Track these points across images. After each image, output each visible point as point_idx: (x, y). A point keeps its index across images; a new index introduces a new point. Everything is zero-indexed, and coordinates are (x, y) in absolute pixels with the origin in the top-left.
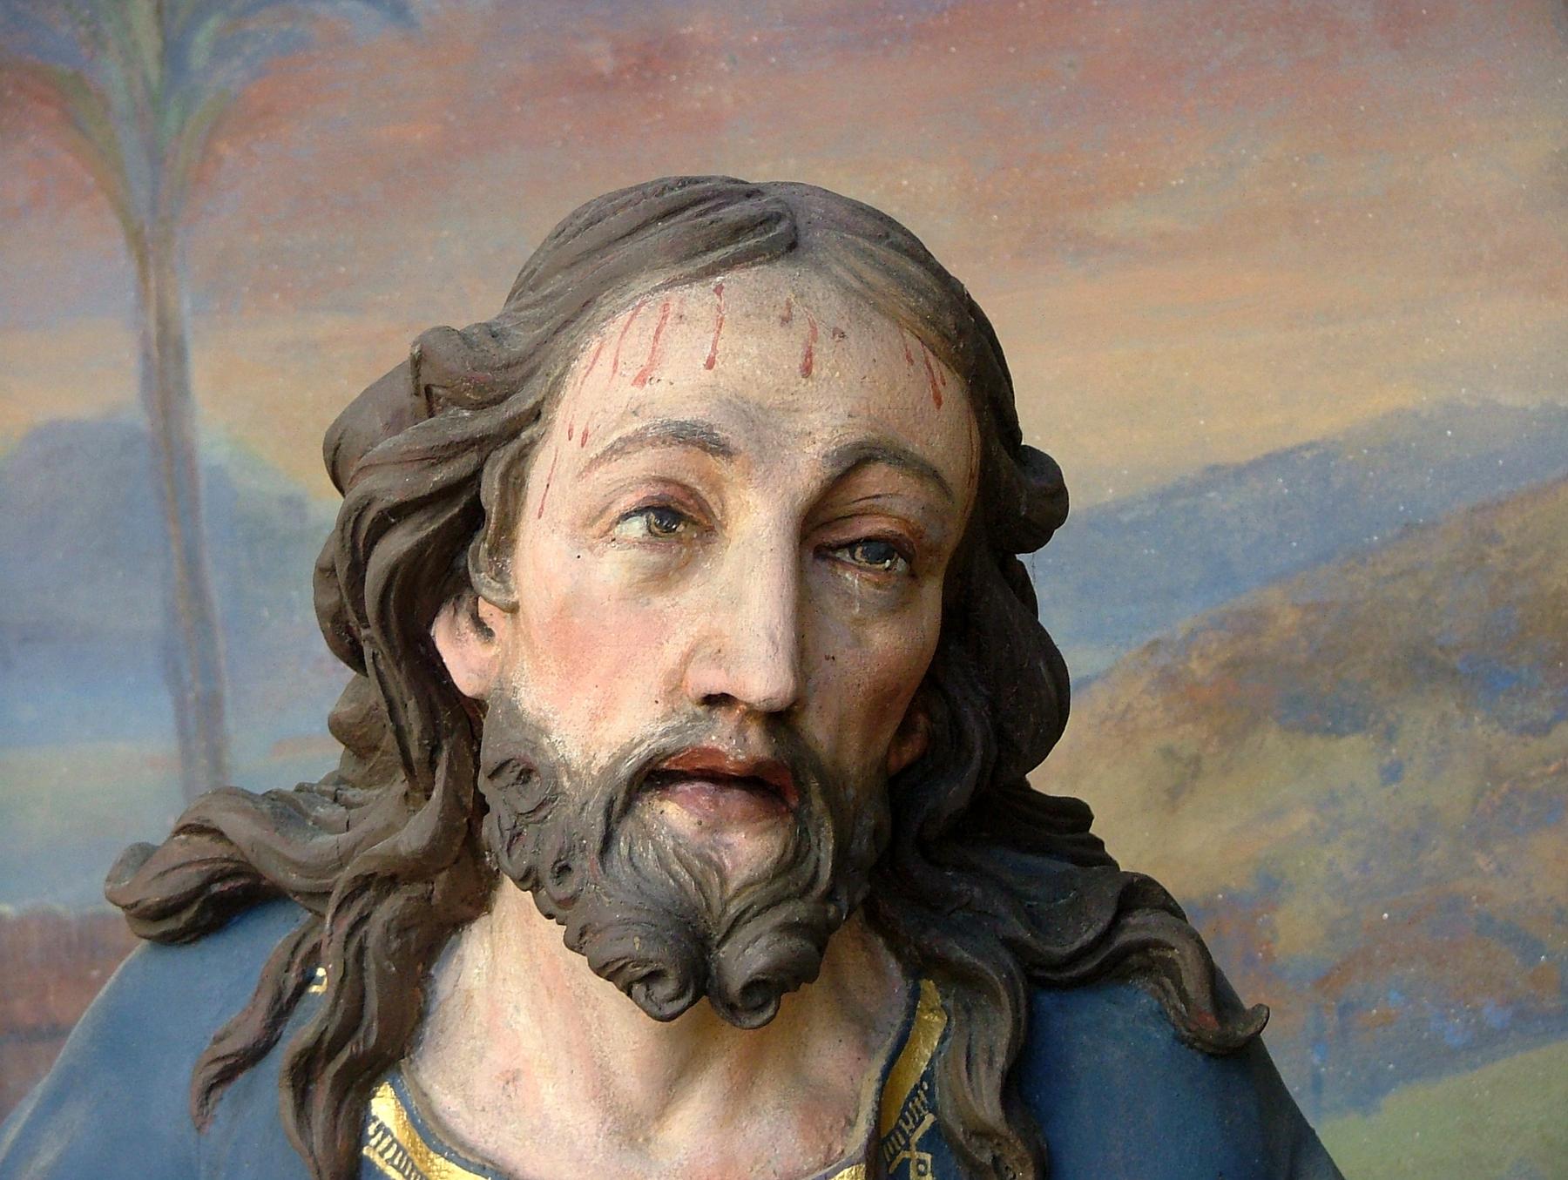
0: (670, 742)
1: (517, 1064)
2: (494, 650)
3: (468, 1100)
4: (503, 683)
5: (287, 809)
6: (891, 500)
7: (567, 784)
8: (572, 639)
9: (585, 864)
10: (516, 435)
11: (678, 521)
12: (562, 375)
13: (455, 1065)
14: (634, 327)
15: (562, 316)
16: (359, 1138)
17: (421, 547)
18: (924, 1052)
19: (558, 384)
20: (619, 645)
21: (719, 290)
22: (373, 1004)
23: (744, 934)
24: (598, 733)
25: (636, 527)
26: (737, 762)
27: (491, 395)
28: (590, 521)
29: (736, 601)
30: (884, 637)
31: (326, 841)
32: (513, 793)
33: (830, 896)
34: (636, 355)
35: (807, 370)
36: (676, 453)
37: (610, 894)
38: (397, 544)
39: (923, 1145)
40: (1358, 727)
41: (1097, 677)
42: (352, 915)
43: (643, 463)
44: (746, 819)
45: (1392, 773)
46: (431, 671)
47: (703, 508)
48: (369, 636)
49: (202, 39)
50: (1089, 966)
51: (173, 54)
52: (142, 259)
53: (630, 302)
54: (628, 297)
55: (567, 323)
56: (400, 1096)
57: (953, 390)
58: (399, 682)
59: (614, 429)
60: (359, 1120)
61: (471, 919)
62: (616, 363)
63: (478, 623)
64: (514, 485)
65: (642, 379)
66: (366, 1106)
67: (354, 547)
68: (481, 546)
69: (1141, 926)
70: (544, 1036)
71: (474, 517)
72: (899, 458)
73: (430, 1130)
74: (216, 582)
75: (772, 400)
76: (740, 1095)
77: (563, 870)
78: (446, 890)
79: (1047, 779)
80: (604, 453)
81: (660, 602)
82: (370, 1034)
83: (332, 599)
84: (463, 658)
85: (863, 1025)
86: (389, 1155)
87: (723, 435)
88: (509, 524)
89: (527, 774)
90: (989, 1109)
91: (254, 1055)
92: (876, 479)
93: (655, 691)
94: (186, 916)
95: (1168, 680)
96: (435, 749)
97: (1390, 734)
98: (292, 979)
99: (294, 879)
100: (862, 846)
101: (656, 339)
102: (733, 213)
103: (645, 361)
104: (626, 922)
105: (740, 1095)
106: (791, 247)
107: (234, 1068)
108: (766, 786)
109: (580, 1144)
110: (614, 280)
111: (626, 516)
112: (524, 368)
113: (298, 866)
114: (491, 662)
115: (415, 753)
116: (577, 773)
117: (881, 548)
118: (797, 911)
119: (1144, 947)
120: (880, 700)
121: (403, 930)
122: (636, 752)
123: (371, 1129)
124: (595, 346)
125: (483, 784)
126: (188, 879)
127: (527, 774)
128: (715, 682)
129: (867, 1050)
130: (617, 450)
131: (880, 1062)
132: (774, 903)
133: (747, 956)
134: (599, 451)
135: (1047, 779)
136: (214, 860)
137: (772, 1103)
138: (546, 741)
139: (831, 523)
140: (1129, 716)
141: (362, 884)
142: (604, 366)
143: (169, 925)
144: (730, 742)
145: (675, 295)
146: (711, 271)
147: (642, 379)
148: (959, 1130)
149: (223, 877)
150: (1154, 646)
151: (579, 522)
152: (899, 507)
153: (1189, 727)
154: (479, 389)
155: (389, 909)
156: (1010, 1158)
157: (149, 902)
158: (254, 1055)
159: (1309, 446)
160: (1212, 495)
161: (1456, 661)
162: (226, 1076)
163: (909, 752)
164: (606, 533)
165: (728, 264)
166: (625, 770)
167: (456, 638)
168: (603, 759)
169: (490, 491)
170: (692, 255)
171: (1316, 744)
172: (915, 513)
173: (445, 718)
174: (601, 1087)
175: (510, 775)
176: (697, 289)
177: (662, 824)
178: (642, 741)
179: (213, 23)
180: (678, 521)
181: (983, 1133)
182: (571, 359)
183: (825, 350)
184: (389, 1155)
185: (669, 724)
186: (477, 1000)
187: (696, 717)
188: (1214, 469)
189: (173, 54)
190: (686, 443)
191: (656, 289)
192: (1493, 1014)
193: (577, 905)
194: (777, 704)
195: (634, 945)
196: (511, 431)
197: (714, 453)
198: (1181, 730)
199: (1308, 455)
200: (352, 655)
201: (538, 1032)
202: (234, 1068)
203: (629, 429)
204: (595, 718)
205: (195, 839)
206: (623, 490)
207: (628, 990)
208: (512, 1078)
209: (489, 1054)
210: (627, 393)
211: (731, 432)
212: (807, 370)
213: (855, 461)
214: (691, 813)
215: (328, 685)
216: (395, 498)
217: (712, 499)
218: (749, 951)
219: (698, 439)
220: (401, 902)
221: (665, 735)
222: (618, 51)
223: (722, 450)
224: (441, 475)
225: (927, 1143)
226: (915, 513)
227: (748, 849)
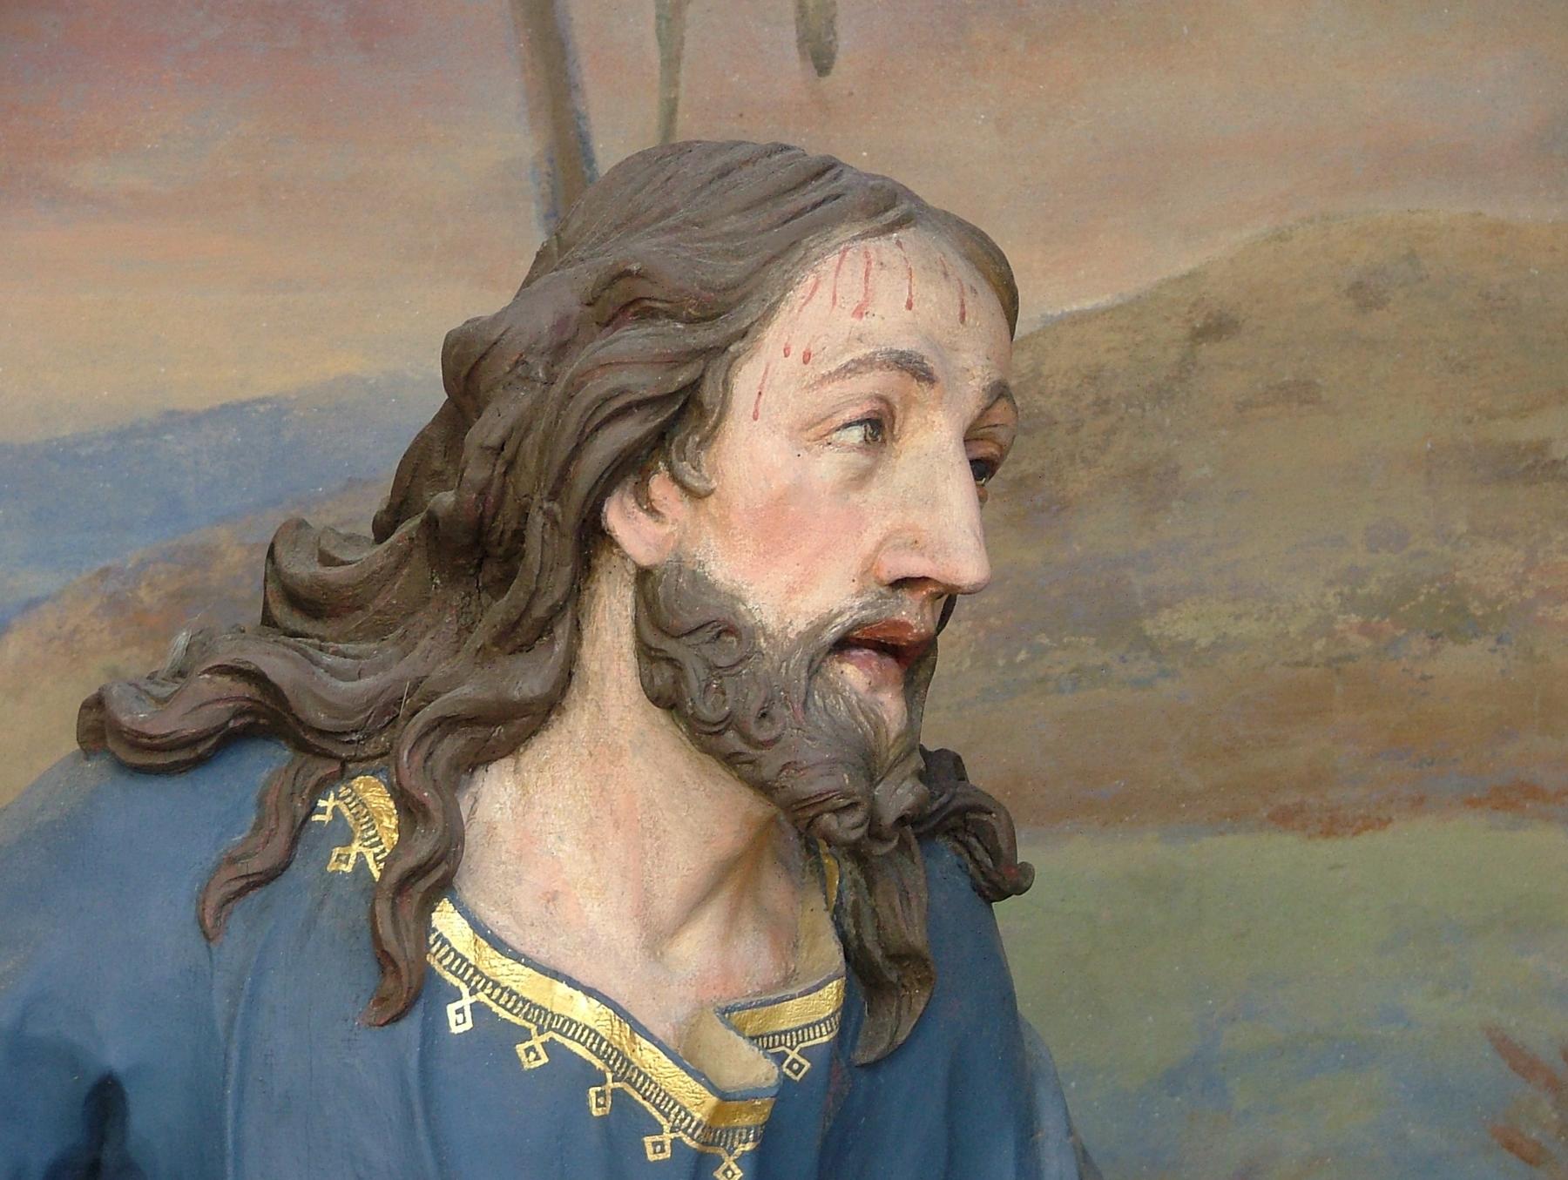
1: (557, 886)
2: (668, 529)
3: (515, 915)
7: (764, 645)
8: (779, 521)
12: (779, 301)
13: (492, 886)
14: (846, 266)
15: (768, 252)
19: (773, 308)
21: (899, 244)
24: (794, 604)
25: (856, 435)
26: (918, 635)
27: (710, 313)
28: (809, 426)
29: (931, 502)
32: (707, 650)
34: (852, 291)
36: (894, 376)
41: (47, 598)
42: (423, 751)
43: (871, 382)
53: (835, 247)
54: (834, 242)
55: (774, 258)
59: (842, 353)
62: (835, 297)
65: (860, 312)
66: (430, 921)
67: (583, 431)
70: (594, 861)
80: (838, 371)
81: (855, 498)
86: (446, 962)
87: (930, 365)
93: (854, 571)
95: (116, 605)
101: (867, 281)
103: (861, 298)
104: (834, 762)
109: (624, 954)
111: (847, 425)
113: (328, 706)
114: (666, 538)
116: (772, 636)
122: (839, 620)
123: (432, 938)
124: (811, 280)
127: (730, 630)
128: (914, 565)
134: (833, 368)
136: (237, 698)
137: (750, 926)
138: (743, 608)
140: (78, 637)
145: (872, 244)
147: (860, 312)
148: (878, 954)
150: (104, 573)
151: (798, 426)
153: (135, 650)
154: (701, 306)
157: (185, 733)
159: (263, 401)
160: (168, 437)
164: (822, 437)
167: (627, 516)
168: (801, 625)
169: (708, 393)
174: (643, 908)
177: (844, 681)
178: (840, 614)
182: (787, 289)
184: (446, 962)
185: (863, 599)
186: (501, 830)
187: (882, 596)
188: (171, 414)
190: (902, 369)
191: (855, 239)
193: (778, 745)
197: (920, 379)
198: (126, 653)
199: (261, 409)
201: (588, 858)
203: (861, 352)
204: (791, 591)
205: (218, 679)
206: (852, 403)
208: (552, 897)
209: (529, 877)
210: (847, 323)
214: (866, 675)
217: (899, 416)
218: (899, 791)
220: (461, 742)
221: (863, 608)
224: (683, 377)
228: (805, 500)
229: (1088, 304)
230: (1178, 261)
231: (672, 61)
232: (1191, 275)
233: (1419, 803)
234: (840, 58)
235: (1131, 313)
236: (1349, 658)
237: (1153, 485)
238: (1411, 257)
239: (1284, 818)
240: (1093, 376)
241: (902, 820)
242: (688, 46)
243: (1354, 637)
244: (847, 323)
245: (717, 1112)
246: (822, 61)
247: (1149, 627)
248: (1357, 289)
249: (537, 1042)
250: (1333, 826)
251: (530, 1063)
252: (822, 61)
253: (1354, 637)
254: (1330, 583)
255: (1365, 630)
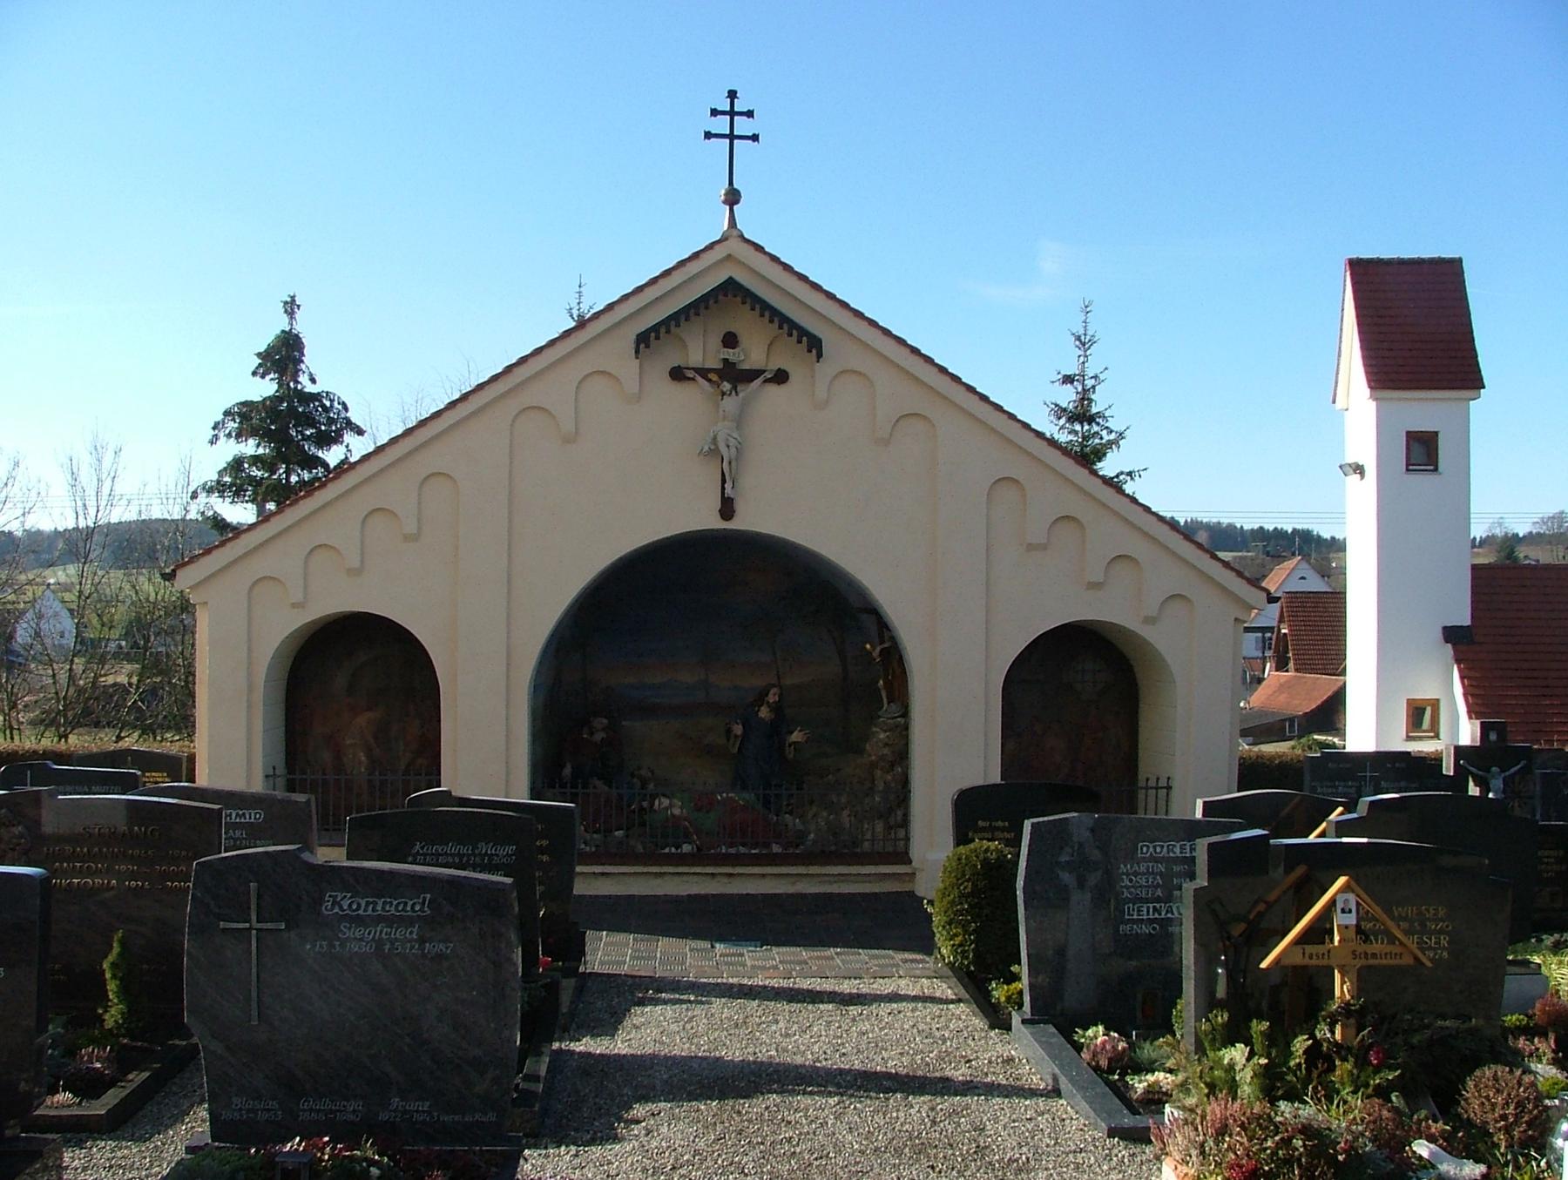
228: (772, 697)
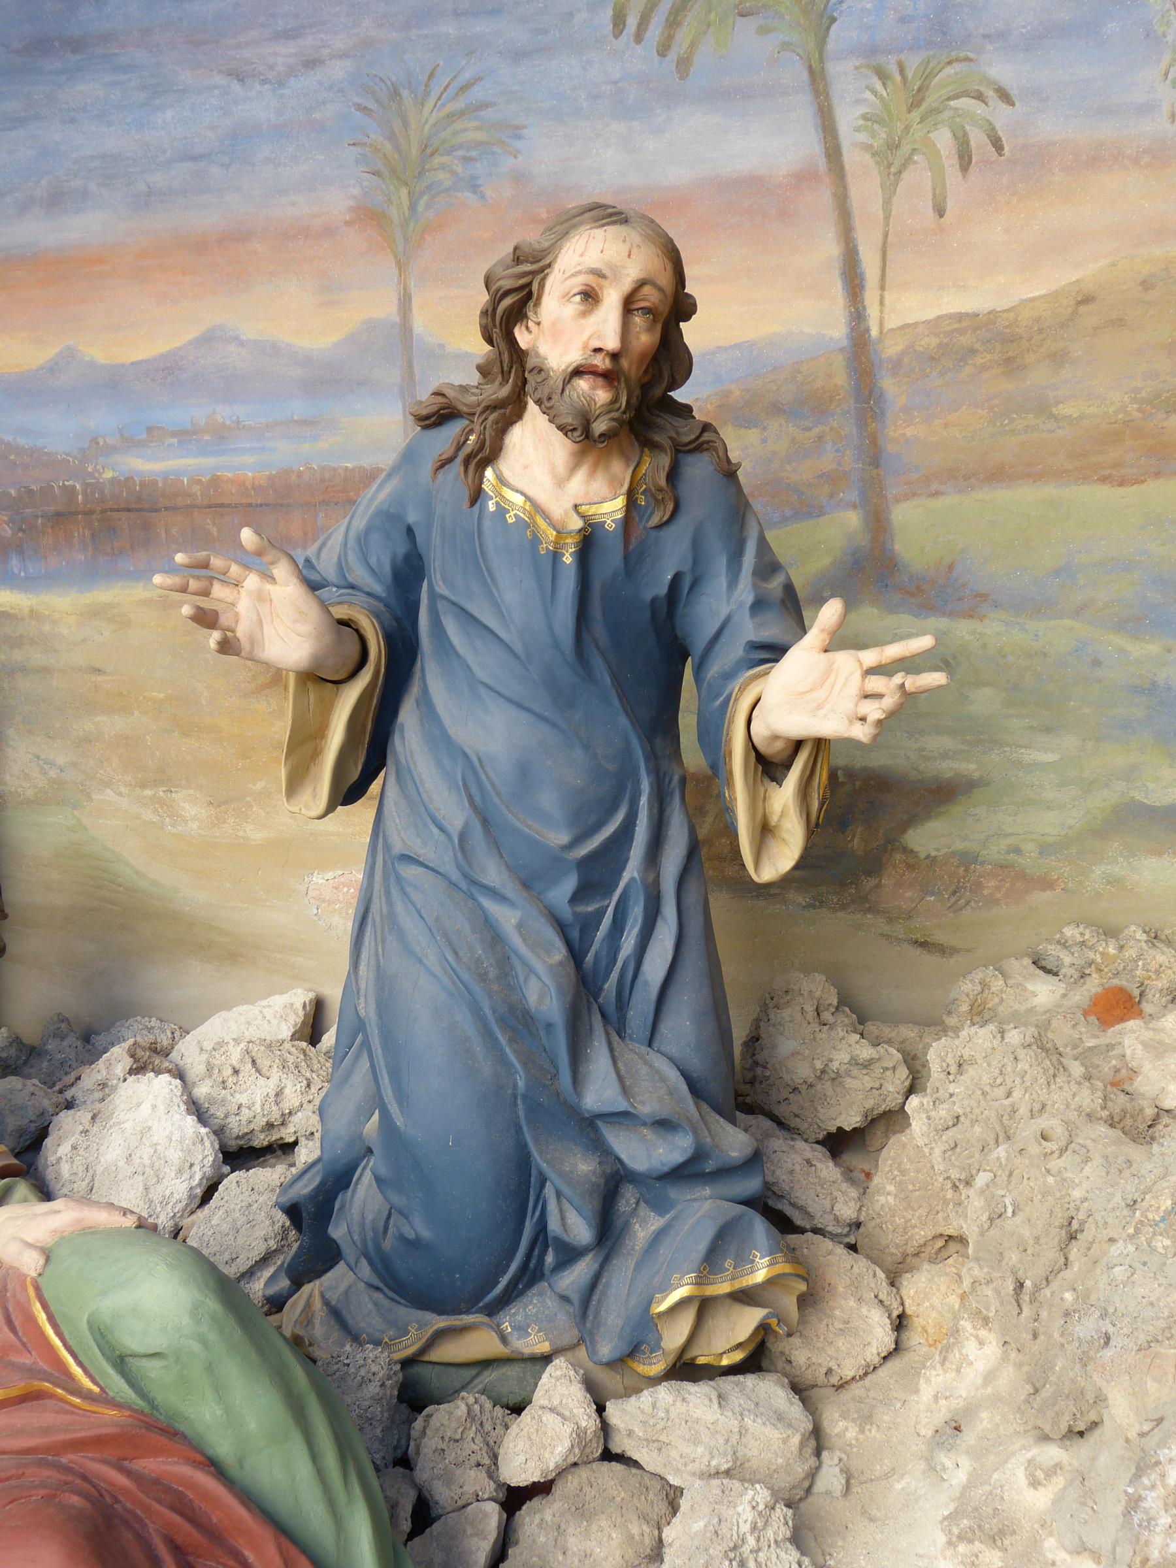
0: (584, 362)
4: (534, 346)
5: (464, 389)
6: (650, 296)
8: (556, 332)
9: (555, 397)
10: (544, 271)
11: (590, 297)
16: (481, 482)
17: (514, 303)
18: (643, 469)
19: (556, 257)
20: (568, 334)
22: (488, 443)
23: (601, 419)
28: (564, 296)
29: (605, 321)
30: (645, 339)
31: (474, 398)
33: (624, 412)
35: (629, 256)
37: (564, 406)
38: (508, 302)
39: (643, 493)
40: (756, 427)
44: (603, 387)
45: (764, 441)
46: (512, 342)
47: (597, 295)
48: (496, 333)
49: (422, 202)
50: (692, 446)
51: (413, 207)
52: (400, 270)
56: (494, 471)
57: (669, 267)
58: (503, 345)
60: (482, 477)
61: (516, 422)
63: (527, 328)
64: (542, 286)
65: (582, 255)
68: (531, 304)
69: (707, 436)
71: (529, 295)
72: (654, 285)
73: (501, 480)
74: (417, 369)
75: (619, 264)
76: (592, 473)
77: (550, 399)
78: (510, 411)
79: (680, 395)
81: (582, 321)
82: (487, 450)
83: (484, 321)
84: (523, 338)
85: (627, 459)
88: (539, 298)
89: (541, 370)
90: (662, 482)
91: (450, 460)
92: (647, 290)
94: (433, 419)
96: (511, 367)
97: (765, 429)
98: (463, 439)
99: (465, 409)
100: (634, 400)
102: (610, 211)
105: (592, 473)
106: (626, 221)
107: (444, 463)
108: (608, 377)
110: (574, 227)
112: (546, 252)
113: (466, 405)
115: (505, 368)
117: (647, 311)
118: (615, 415)
119: (708, 442)
120: (643, 356)
121: (497, 423)
125: (526, 375)
126: (434, 408)
127: (541, 370)
128: (598, 345)
129: (628, 466)
130: (573, 275)
131: (631, 469)
132: (610, 412)
133: (600, 426)
135: (680, 395)
139: (632, 303)
141: (487, 408)
142: (570, 252)
143: (427, 422)
144: (602, 363)
146: (603, 225)
149: (444, 409)
152: (652, 299)
155: (494, 416)
156: (667, 498)
158: (450, 460)
161: (786, 408)
162: (442, 466)
163: (647, 378)
165: (608, 224)
166: (570, 370)
167: (521, 333)
168: (563, 367)
170: (598, 220)
171: (742, 431)
172: (657, 301)
173: (515, 357)
175: (535, 372)
176: (599, 230)
179: (426, 197)
180: (590, 297)
181: (660, 490)
183: (634, 251)
189: (413, 207)
192: (788, 512)
194: (616, 351)
195: (569, 420)
196: (542, 270)
200: (489, 340)
202: (444, 463)
207: (566, 435)
210: (577, 259)
211: (606, 271)
212: (629, 256)
213: (641, 284)
215: (481, 349)
216: (508, 288)
219: (598, 274)
222: (548, 212)
223: (604, 277)
224: (521, 282)
225: (643, 493)
226: (657, 301)
227: (602, 396)
229: (1036, 294)
230: (1071, 276)
231: (887, 218)
232: (1077, 281)
233: (1157, 475)
234: (948, 213)
235: (1053, 296)
236: (1132, 421)
237: (1058, 359)
238: (1166, 269)
239: (1104, 480)
240: (1038, 320)
241: (602, 435)
242: (893, 212)
243: (1135, 413)
244: (577, 259)
245: (557, 537)
246: (941, 212)
247: (1054, 411)
248: (1143, 283)
249: (512, 513)
250: (1121, 484)
251: (510, 521)
252: (941, 212)
253: (1135, 413)
254: (1126, 393)
255: (1139, 410)
